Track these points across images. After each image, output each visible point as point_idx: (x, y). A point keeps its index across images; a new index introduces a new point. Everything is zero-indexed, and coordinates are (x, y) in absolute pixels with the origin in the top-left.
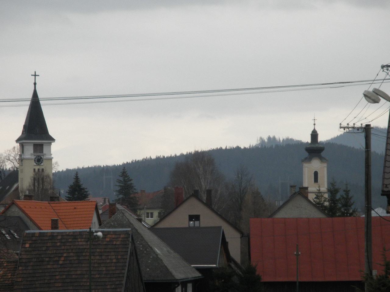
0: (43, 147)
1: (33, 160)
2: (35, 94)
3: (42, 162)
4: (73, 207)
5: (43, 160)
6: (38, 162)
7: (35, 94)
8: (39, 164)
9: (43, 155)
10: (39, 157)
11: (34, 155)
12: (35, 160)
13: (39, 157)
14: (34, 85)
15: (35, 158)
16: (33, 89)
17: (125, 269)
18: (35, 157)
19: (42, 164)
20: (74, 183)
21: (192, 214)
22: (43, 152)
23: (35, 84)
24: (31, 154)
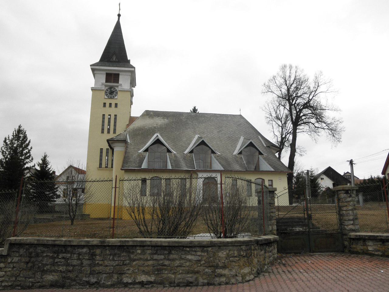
0: (119, 77)
1: (104, 92)
2: (118, 27)
3: (116, 95)
4: (295, 283)
5: (117, 93)
6: (112, 95)
7: (118, 27)
8: (107, 92)
9: (117, 86)
10: (111, 97)
11: (106, 86)
12: (106, 92)
13: (111, 97)
14: (117, 17)
15: (107, 90)
16: (117, 20)
17: (306, 171)
18: (107, 88)
19: (116, 98)
20: (303, 172)
21: (107, 124)
22: (118, 82)
23: (119, 15)
24: (103, 84)
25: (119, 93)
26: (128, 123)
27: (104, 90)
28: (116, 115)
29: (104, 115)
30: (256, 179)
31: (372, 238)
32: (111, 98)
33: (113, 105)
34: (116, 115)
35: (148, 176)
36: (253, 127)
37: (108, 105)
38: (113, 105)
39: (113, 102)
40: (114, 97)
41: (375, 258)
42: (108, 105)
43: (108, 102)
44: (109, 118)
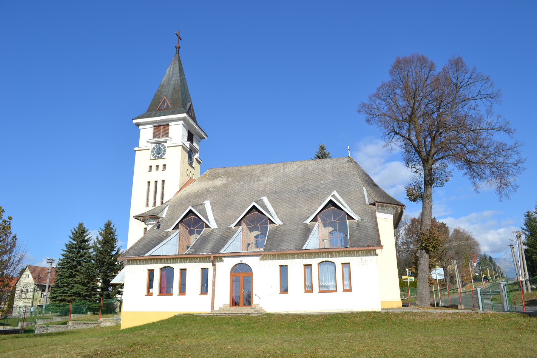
3: (164, 154)
10: (158, 157)
13: (158, 157)
15: (154, 148)
25: (168, 149)
26: (178, 191)
27: (149, 149)
28: (163, 181)
29: (149, 182)
30: (320, 263)
31: (62, 334)
32: (158, 158)
33: (161, 167)
34: (163, 181)
35: (314, 262)
36: (159, 322)
37: (154, 168)
38: (161, 167)
39: (160, 162)
40: (161, 156)
41: (62, 322)
42: (154, 168)
43: (154, 163)
44: (152, 287)
